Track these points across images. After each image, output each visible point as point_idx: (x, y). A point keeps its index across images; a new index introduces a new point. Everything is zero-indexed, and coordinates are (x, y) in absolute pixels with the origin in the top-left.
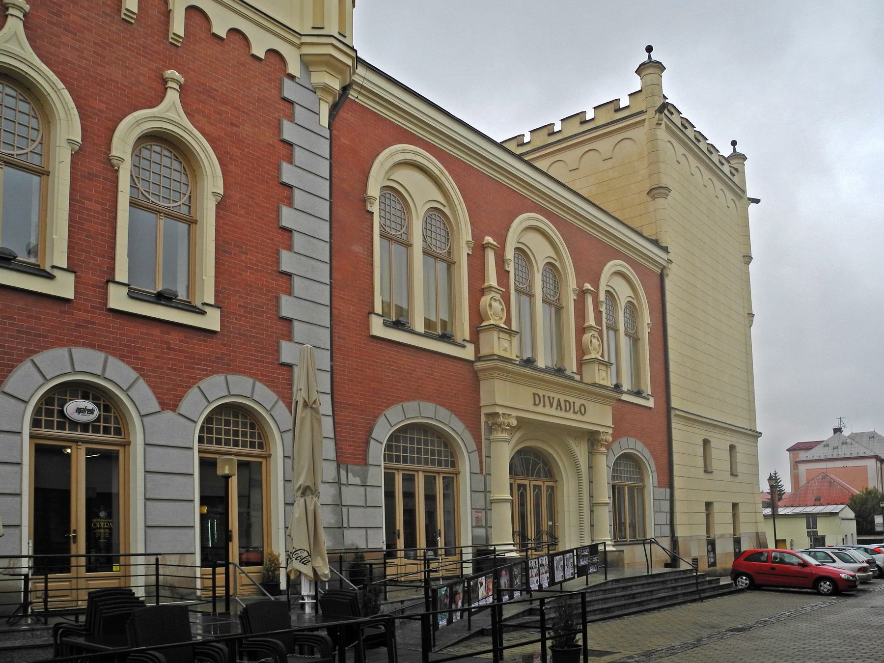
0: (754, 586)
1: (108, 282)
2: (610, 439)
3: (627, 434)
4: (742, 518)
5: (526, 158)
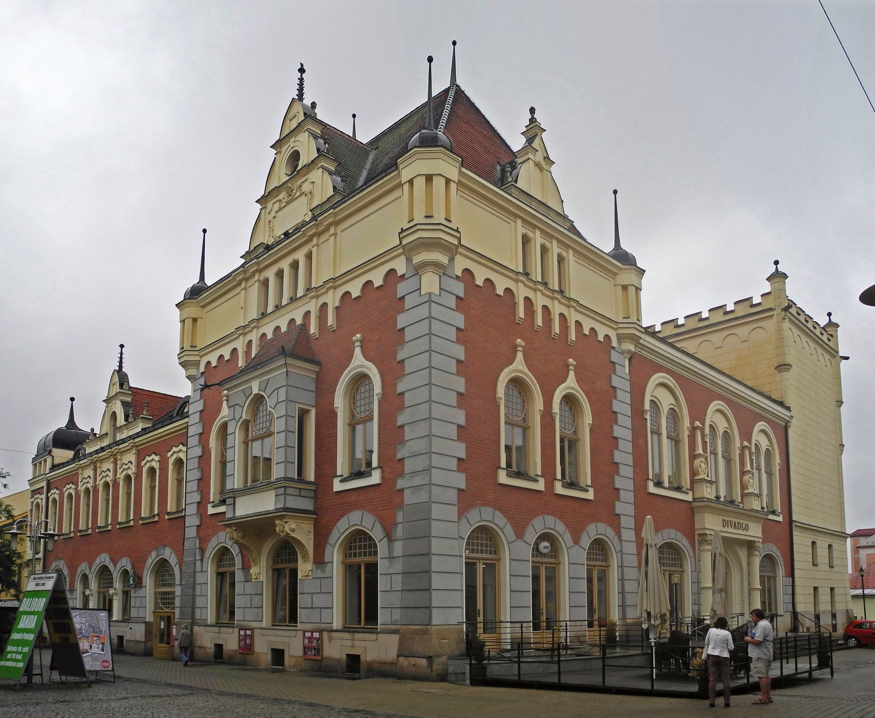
0: (860, 645)
4: (837, 598)
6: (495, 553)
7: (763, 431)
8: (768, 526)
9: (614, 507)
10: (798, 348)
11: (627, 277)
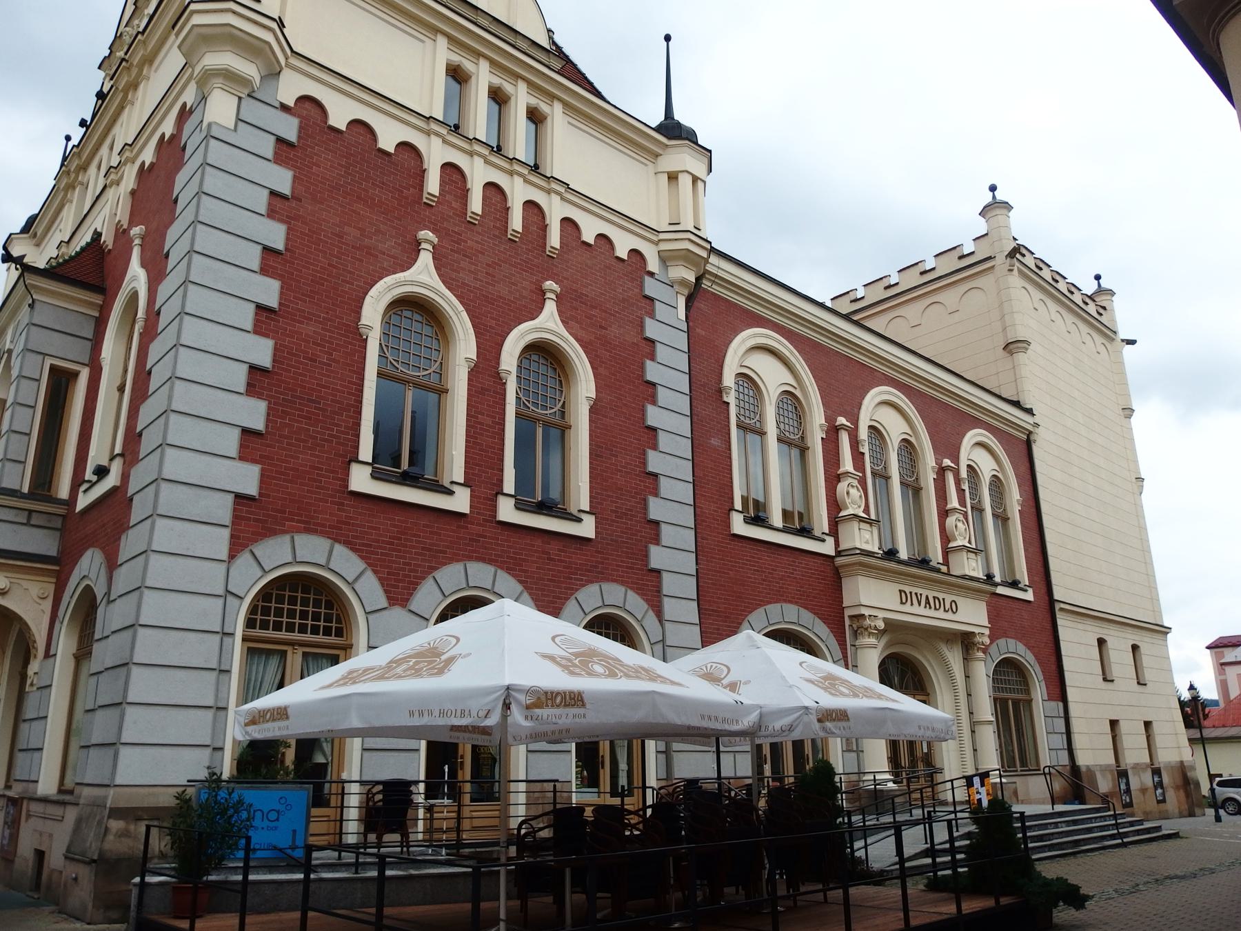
1: (497, 494)
2: (987, 641)
3: (1005, 635)
4: (1159, 741)
5: (855, 318)
6: (339, 633)
7: (979, 444)
8: (1000, 610)
9: (646, 556)
10: (1031, 314)
11: (680, 158)
